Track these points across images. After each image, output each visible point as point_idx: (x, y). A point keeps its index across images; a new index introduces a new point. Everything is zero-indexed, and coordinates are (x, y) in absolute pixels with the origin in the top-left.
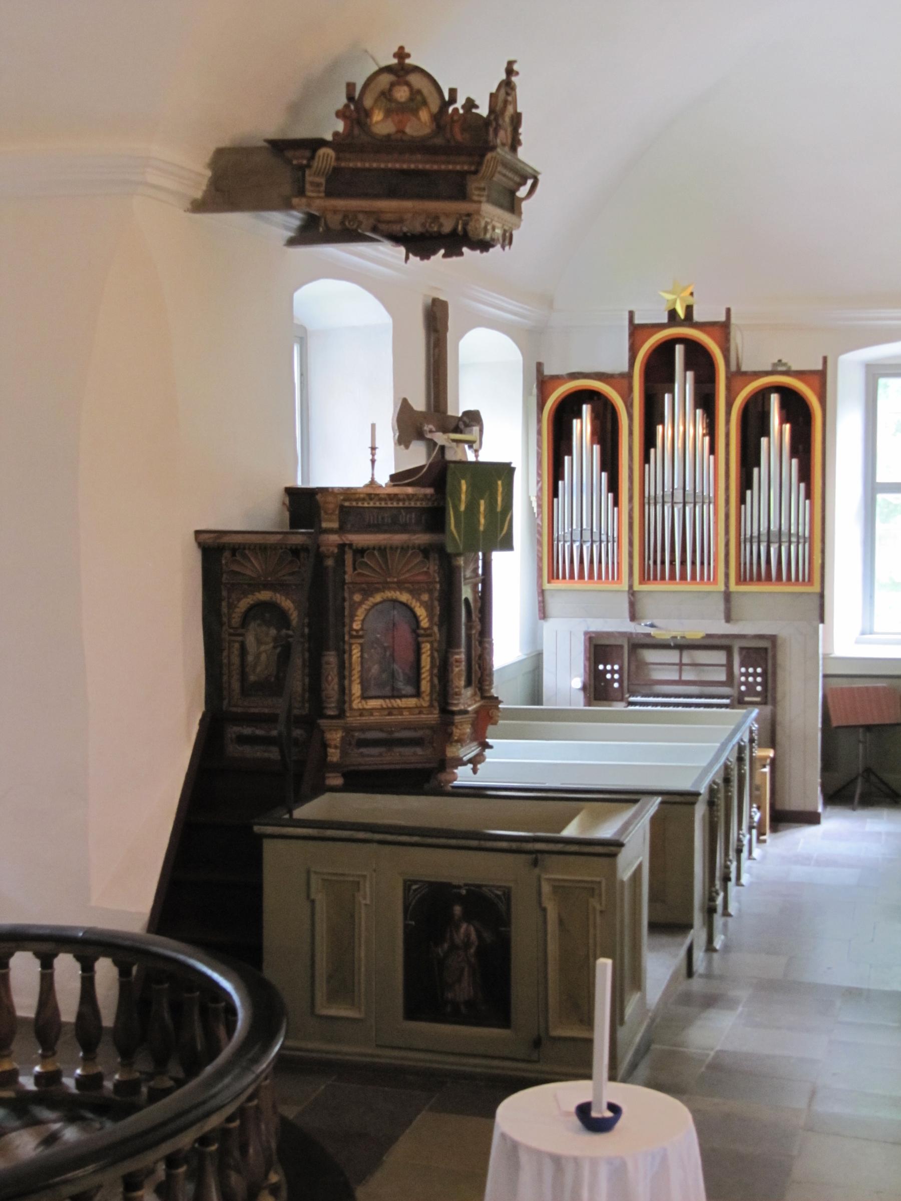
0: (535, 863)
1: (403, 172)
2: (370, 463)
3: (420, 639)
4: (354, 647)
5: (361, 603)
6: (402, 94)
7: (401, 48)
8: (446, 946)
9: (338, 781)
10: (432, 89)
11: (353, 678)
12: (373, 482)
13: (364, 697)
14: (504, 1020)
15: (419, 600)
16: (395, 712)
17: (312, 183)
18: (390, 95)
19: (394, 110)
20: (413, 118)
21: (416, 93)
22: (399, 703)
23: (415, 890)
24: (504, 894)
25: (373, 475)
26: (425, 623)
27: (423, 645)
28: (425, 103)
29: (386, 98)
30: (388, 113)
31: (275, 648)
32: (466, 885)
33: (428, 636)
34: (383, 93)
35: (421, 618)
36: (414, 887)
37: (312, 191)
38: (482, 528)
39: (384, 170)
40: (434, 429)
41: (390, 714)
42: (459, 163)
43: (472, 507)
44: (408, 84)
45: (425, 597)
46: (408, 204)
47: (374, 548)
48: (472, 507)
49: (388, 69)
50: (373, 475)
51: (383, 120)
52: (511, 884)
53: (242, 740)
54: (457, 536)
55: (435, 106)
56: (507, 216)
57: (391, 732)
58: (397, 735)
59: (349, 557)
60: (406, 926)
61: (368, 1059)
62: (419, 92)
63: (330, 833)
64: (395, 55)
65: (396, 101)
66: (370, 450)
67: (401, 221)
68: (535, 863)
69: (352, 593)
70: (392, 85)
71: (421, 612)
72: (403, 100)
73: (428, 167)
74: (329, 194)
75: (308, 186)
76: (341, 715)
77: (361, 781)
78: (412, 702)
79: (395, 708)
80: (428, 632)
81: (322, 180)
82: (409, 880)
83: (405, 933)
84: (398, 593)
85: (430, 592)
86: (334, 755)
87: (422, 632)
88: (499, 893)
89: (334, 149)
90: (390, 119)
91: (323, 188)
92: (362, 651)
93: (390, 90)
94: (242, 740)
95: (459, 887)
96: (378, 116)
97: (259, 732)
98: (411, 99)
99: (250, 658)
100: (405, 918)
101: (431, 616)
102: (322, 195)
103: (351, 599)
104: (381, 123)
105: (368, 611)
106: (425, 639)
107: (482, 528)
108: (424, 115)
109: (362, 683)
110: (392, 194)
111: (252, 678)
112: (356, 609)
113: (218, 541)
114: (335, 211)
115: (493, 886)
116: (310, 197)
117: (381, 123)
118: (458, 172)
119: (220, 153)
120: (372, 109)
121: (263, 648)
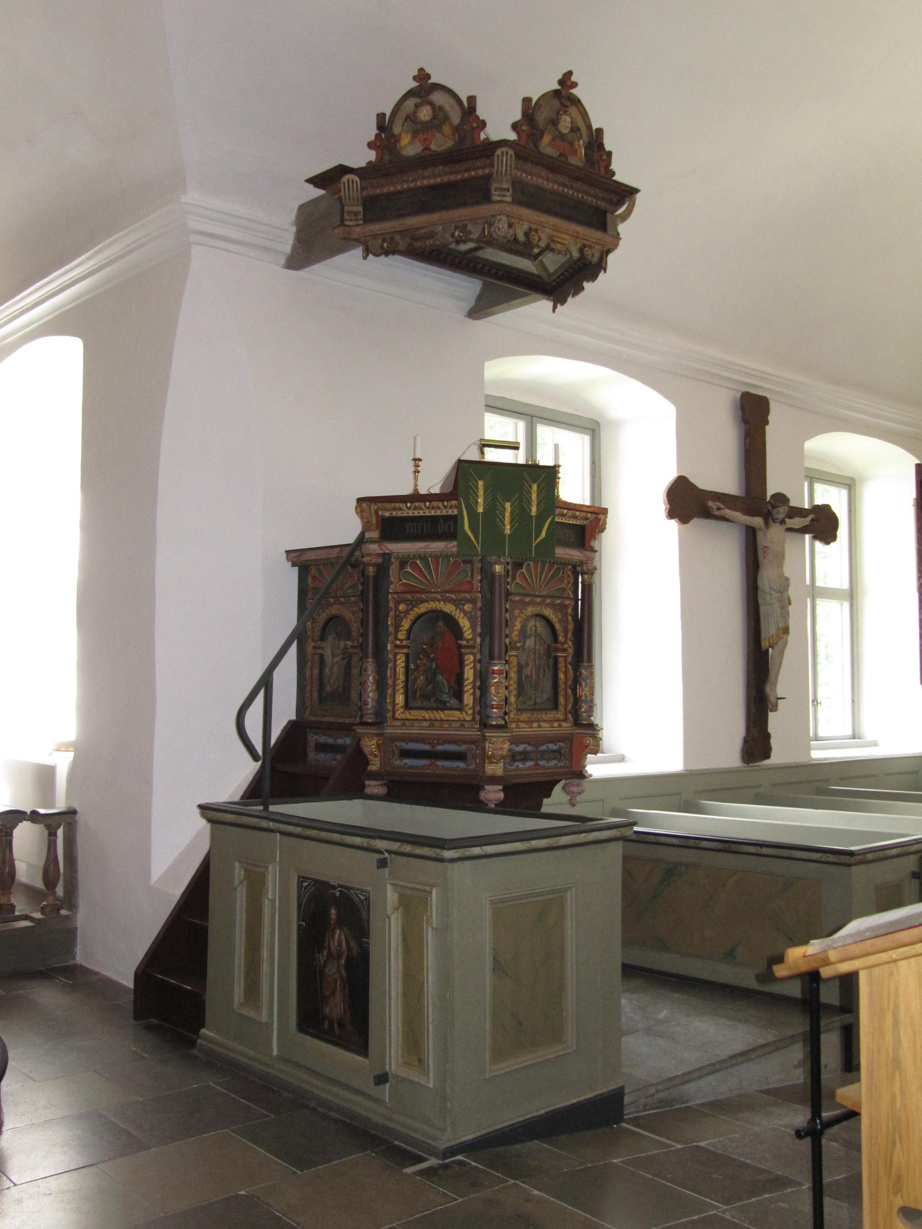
0: (382, 864)
1: (434, 188)
2: (412, 476)
3: (463, 650)
4: (398, 657)
5: (407, 612)
6: (425, 114)
7: (421, 70)
8: (325, 953)
9: (382, 791)
10: (453, 102)
11: (397, 688)
12: (416, 490)
13: (407, 706)
14: (363, 1048)
15: (463, 611)
16: (436, 724)
17: (349, 213)
18: (416, 117)
19: (420, 129)
20: (438, 135)
21: (437, 110)
22: (441, 715)
23: (307, 887)
24: (366, 899)
25: (416, 485)
26: (468, 634)
27: (466, 657)
28: (447, 118)
29: (411, 120)
30: (415, 134)
31: (343, 659)
32: (340, 886)
33: (468, 647)
34: (408, 117)
35: (465, 629)
36: (305, 884)
37: (350, 220)
38: (508, 530)
39: (416, 189)
40: (722, 506)
41: (432, 726)
42: (479, 168)
43: (493, 510)
44: (431, 104)
45: (468, 607)
46: (435, 217)
47: (414, 557)
48: (493, 510)
49: (410, 94)
50: (416, 485)
51: (410, 143)
52: (370, 889)
53: (322, 748)
54: (473, 539)
55: (456, 119)
56: (597, 234)
57: (433, 746)
58: (440, 748)
59: (393, 571)
60: (299, 926)
61: (264, 1068)
62: (441, 108)
63: (324, 835)
64: (415, 78)
65: (422, 123)
66: (412, 463)
67: (432, 235)
68: (382, 864)
69: (397, 603)
70: (417, 106)
71: (465, 623)
72: (427, 118)
73: (452, 178)
74: (368, 220)
75: (346, 217)
76: (380, 720)
77: (403, 790)
78: (457, 714)
79: (436, 720)
80: (471, 643)
81: (360, 209)
82: (303, 877)
83: (298, 934)
84: (442, 603)
85: (473, 601)
86: (375, 765)
87: (464, 643)
88: (362, 898)
89: (362, 178)
90: (417, 141)
91: (361, 216)
92: (407, 662)
93: (415, 112)
94: (322, 748)
95: (334, 888)
96: (405, 140)
97: (330, 741)
98: (435, 117)
99: (327, 670)
100: (298, 920)
101: (473, 627)
102: (361, 222)
103: (397, 608)
104: (409, 147)
105: (414, 622)
106: (468, 650)
107: (508, 530)
108: (447, 129)
109: (406, 694)
110: (425, 209)
111: (328, 689)
112: (401, 620)
113: (301, 559)
114: (375, 236)
115: (359, 889)
116: (349, 226)
117: (409, 147)
118: (481, 177)
119: (302, 208)
120: (400, 134)
121: (336, 659)
